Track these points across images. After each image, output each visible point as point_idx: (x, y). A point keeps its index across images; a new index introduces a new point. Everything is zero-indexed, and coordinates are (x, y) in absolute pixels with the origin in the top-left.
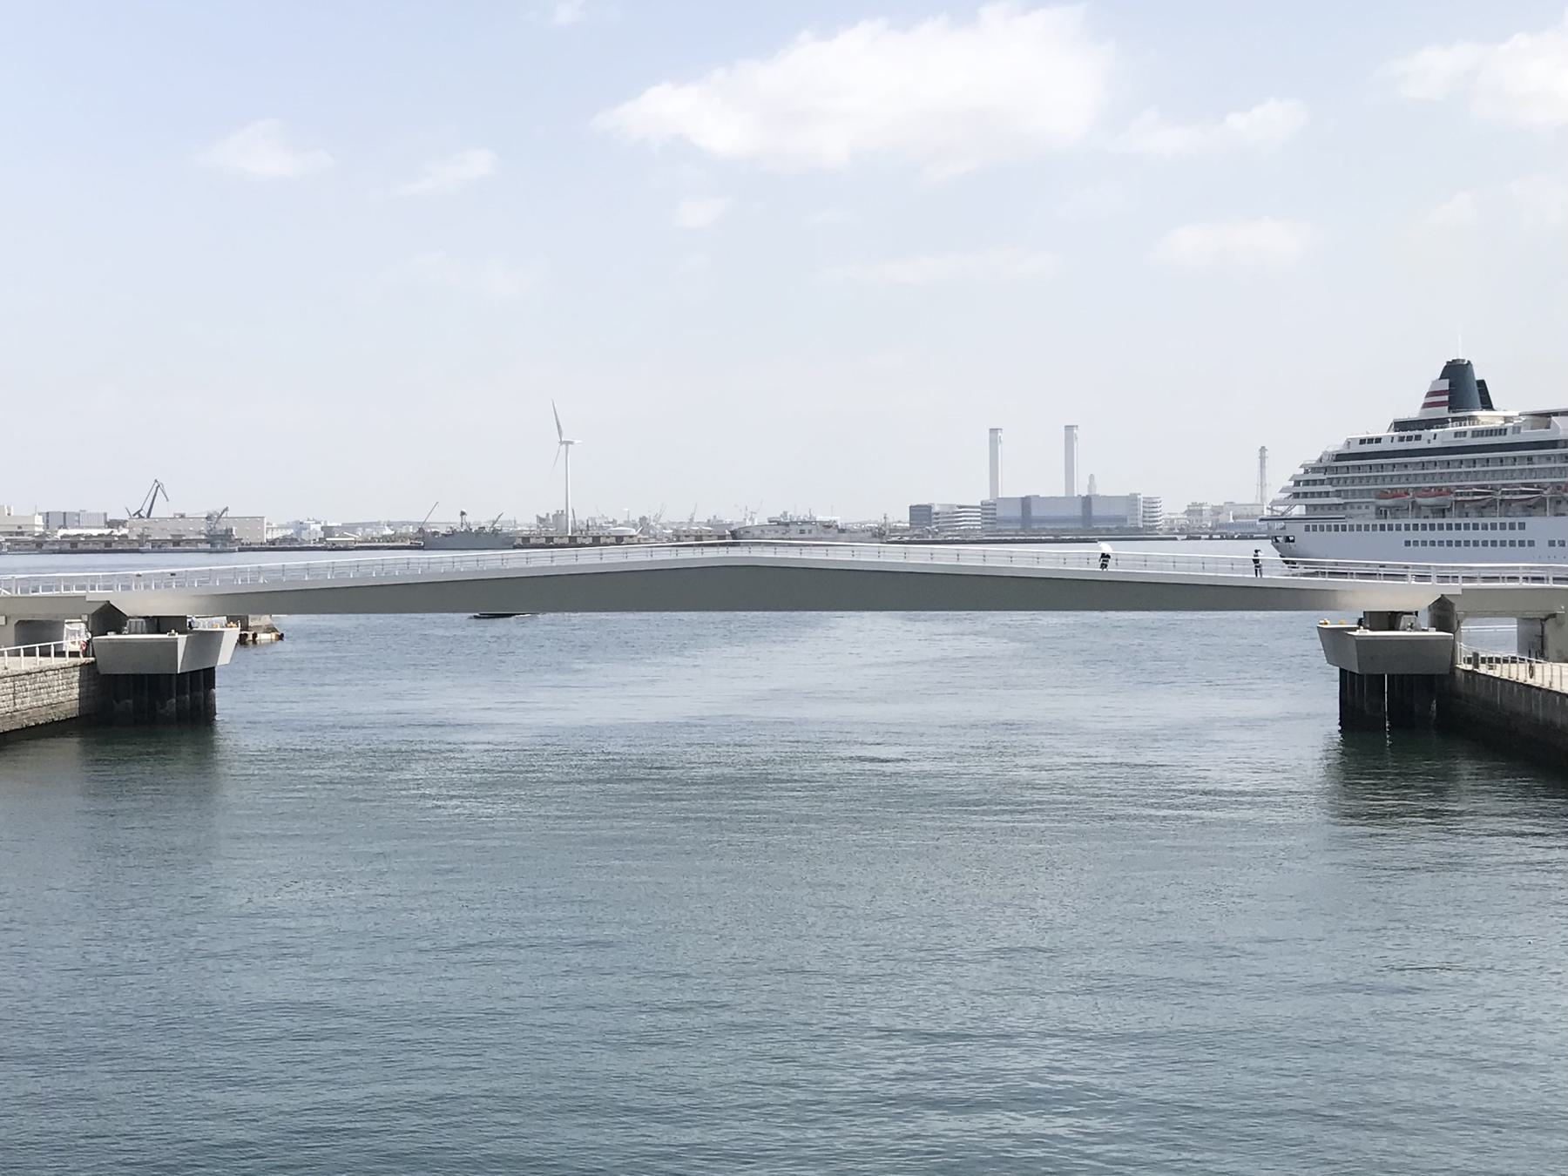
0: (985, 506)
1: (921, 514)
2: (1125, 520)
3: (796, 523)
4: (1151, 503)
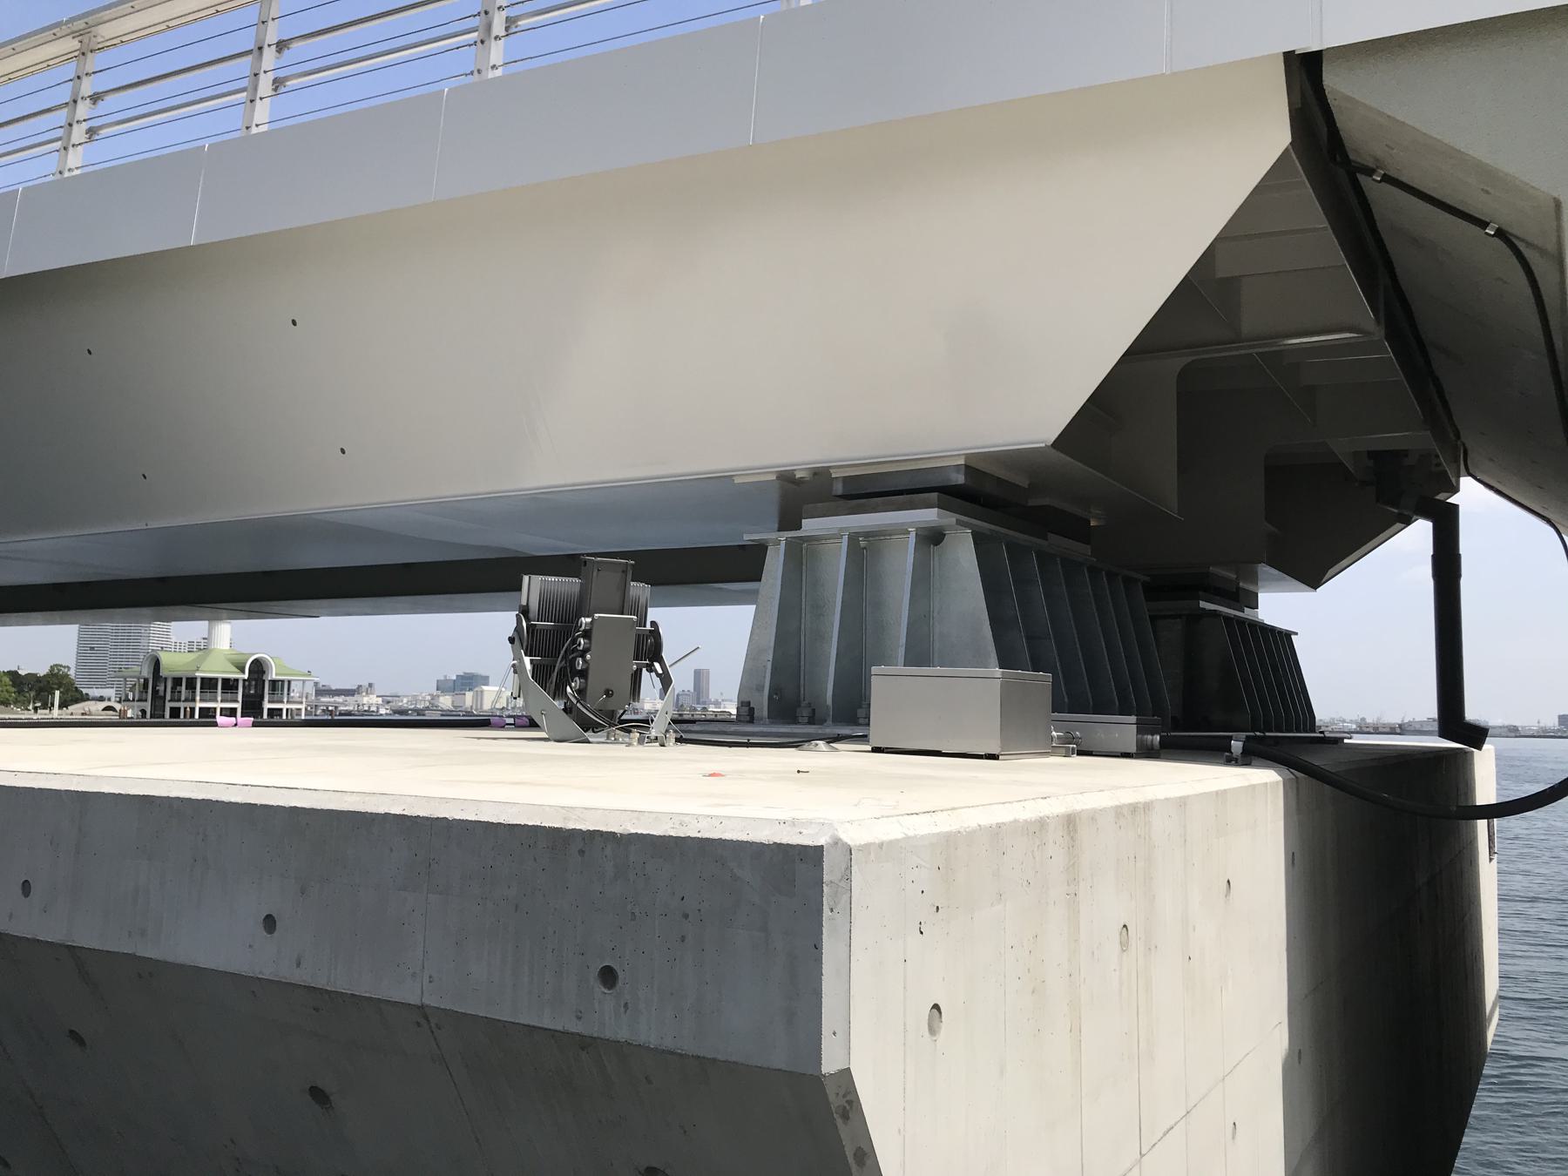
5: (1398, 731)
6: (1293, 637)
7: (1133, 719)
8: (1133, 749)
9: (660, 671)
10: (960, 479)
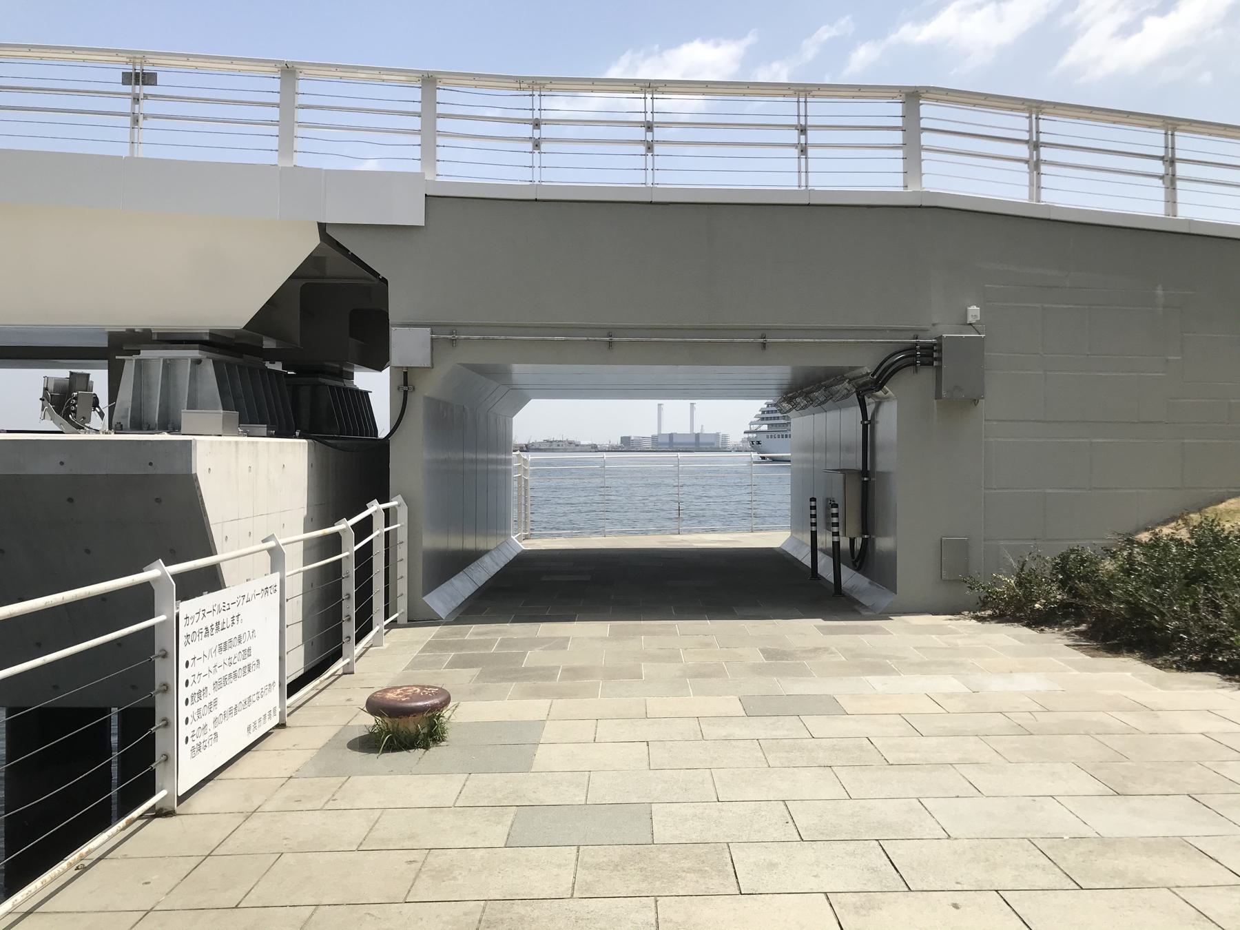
0: (654, 438)
1: (625, 440)
2: (714, 444)
3: (556, 441)
4: (725, 437)
5: (525, 449)
6: (369, 394)
7: (266, 426)
8: (266, 435)
9: (99, 411)
10: (207, 338)
